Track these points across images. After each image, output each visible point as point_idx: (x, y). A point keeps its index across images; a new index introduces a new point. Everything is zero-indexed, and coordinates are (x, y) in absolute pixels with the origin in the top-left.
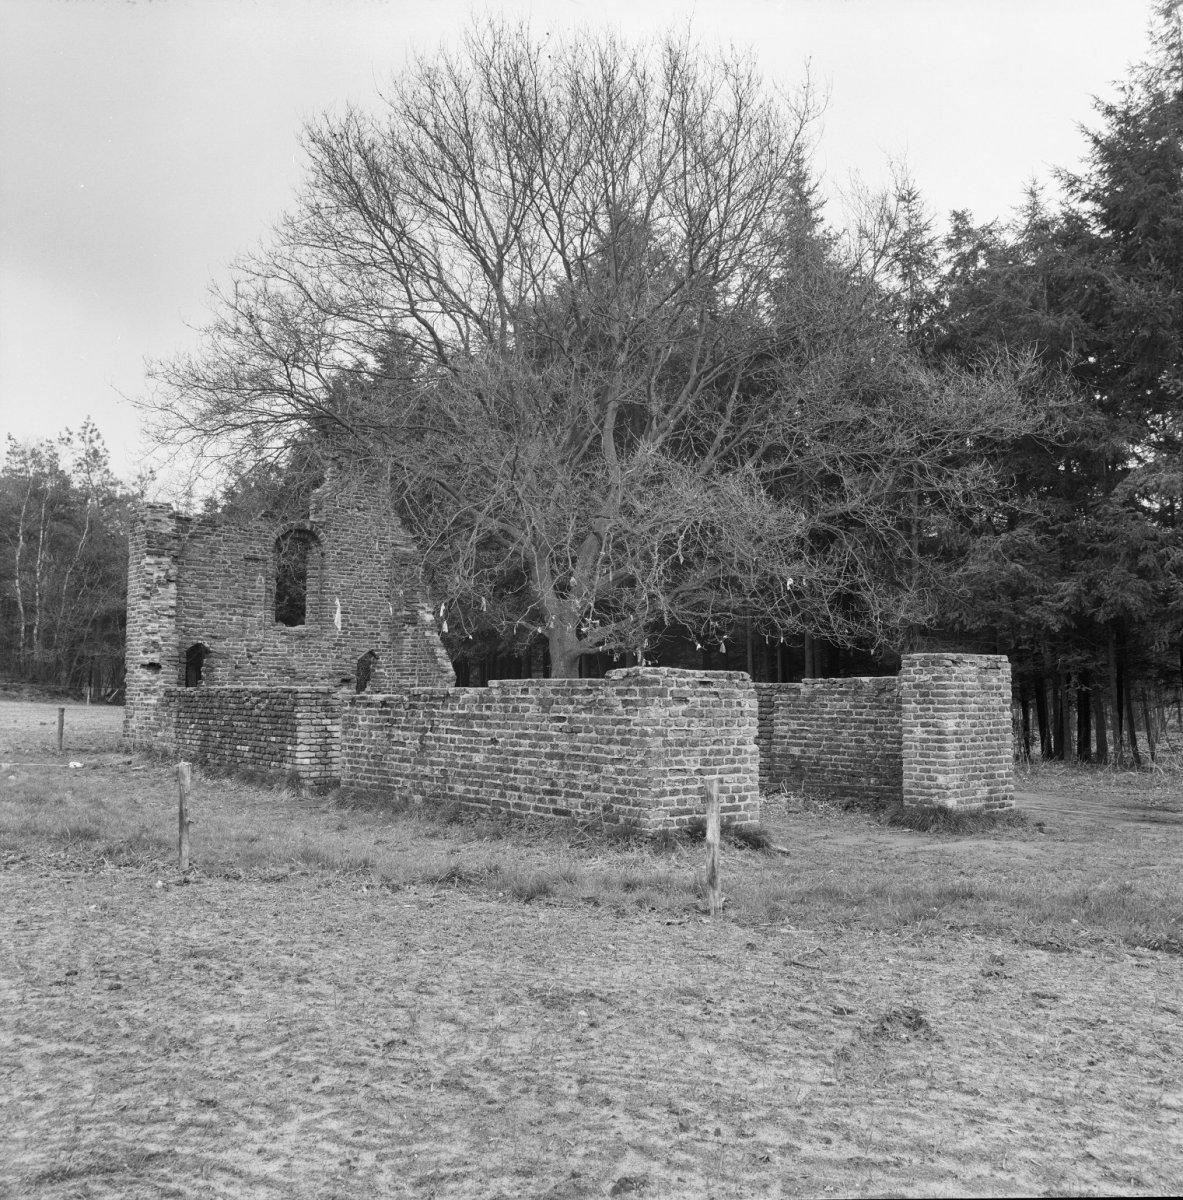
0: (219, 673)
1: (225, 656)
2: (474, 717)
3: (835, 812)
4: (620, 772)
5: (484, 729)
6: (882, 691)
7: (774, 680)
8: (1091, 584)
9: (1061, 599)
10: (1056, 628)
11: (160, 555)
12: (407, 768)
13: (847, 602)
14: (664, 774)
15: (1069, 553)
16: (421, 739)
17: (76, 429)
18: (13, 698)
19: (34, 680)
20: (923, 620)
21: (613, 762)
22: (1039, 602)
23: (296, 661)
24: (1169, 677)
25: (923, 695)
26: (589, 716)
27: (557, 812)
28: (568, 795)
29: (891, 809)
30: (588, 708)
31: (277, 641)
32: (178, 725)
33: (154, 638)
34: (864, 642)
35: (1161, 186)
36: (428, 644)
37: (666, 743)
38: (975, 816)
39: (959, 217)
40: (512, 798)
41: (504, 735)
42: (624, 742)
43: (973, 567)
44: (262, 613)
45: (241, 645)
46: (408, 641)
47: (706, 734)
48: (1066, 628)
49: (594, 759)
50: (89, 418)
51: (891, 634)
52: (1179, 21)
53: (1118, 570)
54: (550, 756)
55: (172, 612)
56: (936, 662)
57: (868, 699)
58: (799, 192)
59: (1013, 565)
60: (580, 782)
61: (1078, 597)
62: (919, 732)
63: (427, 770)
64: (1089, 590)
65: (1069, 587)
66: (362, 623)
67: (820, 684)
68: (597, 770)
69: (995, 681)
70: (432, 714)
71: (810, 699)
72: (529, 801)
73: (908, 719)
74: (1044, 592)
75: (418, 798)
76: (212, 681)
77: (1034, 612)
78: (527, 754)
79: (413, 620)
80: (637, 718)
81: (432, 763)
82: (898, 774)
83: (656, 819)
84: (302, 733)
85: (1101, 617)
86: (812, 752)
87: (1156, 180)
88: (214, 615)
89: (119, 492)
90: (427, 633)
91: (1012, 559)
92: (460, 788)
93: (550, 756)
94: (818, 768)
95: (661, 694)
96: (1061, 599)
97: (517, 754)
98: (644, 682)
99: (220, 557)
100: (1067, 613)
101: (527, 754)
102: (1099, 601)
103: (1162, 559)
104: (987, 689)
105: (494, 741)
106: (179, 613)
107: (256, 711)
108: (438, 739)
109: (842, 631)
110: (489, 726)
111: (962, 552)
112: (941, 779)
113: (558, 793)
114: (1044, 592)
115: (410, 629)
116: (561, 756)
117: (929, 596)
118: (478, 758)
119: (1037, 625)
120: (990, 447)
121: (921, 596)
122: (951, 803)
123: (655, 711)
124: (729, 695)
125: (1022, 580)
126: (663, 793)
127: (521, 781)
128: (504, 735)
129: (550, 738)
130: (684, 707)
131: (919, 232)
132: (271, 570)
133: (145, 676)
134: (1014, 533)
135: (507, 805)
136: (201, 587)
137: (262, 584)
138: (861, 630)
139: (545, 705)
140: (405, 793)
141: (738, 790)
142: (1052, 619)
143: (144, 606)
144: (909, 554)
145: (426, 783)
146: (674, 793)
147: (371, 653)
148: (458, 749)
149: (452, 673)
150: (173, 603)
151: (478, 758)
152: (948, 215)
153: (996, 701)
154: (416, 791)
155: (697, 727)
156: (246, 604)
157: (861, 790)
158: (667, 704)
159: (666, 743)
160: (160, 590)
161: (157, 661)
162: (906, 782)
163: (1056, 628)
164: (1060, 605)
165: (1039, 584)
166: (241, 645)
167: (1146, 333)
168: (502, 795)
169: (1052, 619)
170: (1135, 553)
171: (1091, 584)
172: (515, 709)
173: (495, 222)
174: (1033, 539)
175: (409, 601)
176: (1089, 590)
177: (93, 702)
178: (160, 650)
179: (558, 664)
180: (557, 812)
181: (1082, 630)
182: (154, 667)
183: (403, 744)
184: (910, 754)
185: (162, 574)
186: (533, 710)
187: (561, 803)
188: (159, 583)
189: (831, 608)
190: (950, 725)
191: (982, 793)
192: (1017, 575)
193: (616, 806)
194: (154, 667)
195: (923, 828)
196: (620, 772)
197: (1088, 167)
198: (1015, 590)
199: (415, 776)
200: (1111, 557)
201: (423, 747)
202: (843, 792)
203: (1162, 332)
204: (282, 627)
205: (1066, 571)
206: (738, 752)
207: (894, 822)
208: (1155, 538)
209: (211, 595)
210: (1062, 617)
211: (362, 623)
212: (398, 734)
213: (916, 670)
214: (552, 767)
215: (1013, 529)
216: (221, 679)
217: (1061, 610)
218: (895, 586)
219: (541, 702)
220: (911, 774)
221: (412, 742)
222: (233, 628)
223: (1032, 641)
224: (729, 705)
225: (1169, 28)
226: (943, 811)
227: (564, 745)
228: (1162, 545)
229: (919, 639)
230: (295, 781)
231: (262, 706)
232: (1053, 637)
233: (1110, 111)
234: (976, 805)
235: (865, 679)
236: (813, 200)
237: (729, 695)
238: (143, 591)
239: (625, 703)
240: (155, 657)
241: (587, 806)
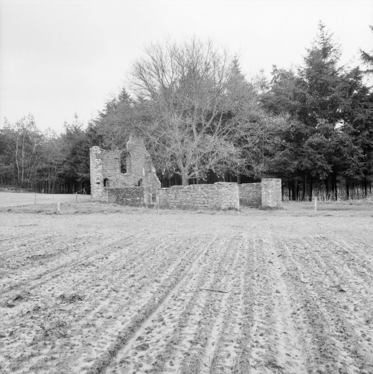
0: (110, 184)
1: (111, 181)
2: (187, 191)
3: (249, 209)
4: (217, 199)
5: (189, 193)
6: (258, 185)
7: (229, 181)
8: (300, 162)
9: (294, 165)
10: (293, 172)
11: (99, 158)
12: (172, 201)
13: (249, 167)
14: (224, 199)
15: (297, 155)
16: (175, 196)
17: (27, 116)
18: (19, 192)
19: (23, 187)
20: (265, 170)
21: (216, 198)
22: (290, 166)
23: (126, 181)
24: (372, 174)
25: (266, 186)
26: (211, 190)
27: (205, 207)
28: (207, 204)
29: (260, 207)
30: (211, 189)
31: (121, 177)
32: (109, 195)
33: (98, 177)
34: (253, 176)
35: (318, 73)
36: (154, 177)
37: (225, 194)
38: (274, 207)
39: (274, 66)
40: (196, 205)
41: (194, 194)
42: (218, 194)
43: (276, 158)
44: (119, 171)
45: (115, 178)
46: (149, 176)
47: (231, 193)
48: (295, 171)
49: (212, 197)
50: (65, 123)
51: (258, 173)
52: (323, 32)
53: (306, 159)
54: (203, 197)
55: (101, 171)
56: (268, 180)
57: (255, 187)
58: (236, 65)
59: (284, 158)
60: (209, 201)
61: (298, 166)
62: (265, 193)
63: (177, 201)
64: (300, 163)
65: (296, 163)
66: (139, 172)
67: (245, 184)
68: (213, 199)
69: (278, 184)
70: (178, 191)
71: (244, 187)
72: (199, 205)
73: (263, 191)
74: (291, 164)
75: (175, 206)
76: (109, 186)
77: (288, 168)
78: (199, 197)
79: (150, 172)
80: (220, 190)
81: (178, 200)
82: (261, 201)
83: (223, 207)
84: (145, 196)
85: (302, 169)
86: (244, 198)
87: (317, 71)
88: (109, 171)
89: (40, 134)
90: (154, 174)
91: (284, 156)
92: (184, 204)
93: (203, 197)
94: (245, 200)
95: (224, 186)
96: (294, 165)
97: (197, 197)
98: (221, 185)
99: (109, 158)
100: (295, 168)
101: (199, 197)
102: (302, 166)
103: (315, 157)
104: (277, 185)
105: (192, 195)
106: (103, 170)
107: (132, 192)
108: (179, 195)
109: (248, 173)
110: (191, 193)
111: (274, 154)
112: (269, 201)
113: (205, 203)
114: (291, 164)
115: (150, 174)
116: (206, 197)
117: (266, 165)
118: (188, 198)
119: (289, 171)
120: (279, 133)
121: (265, 164)
122: (270, 205)
123: (223, 189)
124: (234, 186)
125: (286, 161)
126: (224, 202)
127: (198, 202)
128: (194, 194)
129: (203, 194)
130: (227, 188)
131: (265, 79)
132: (120, 160)
133: (97, 185)
134: (285, 151)
135: (195, 206)
136: (106, 165)
137: (118, 165)
138: (252, 173)
139: (202, 189)
140: (172, 206)
141: (235, 202)
142: (292, 170)
143: (96, 170)
144: (262, 155)
145: (177, 203)
146: (226, 202)
147: (141, 179)
148: (184, 197)
149: (160, 183)
150: (101, 169)
151: (188, 198)
152: (272, 66)
153: (278, 187)
154: (174, 205)
155: (229, 192)
156: (115, 169)
157: (254, 204)
158: (225, 188)
159: (225, 194)
160: (99, 166)
161: (99, 182)
162: (262, 202)
163: (293, 172)
164: (294, 167)
165: (290, 162)
166: (115, 178)
167: (314, 107)
168: (194, 204)
169: (292, 170)
170: (309, 156)
171: (300, 162)
172: (196, 190)
173: (169, 81)
174: (289, 152)
175: (150, 168)
176: (300, 163)
177: (44, 193)
178: (100, 179)
179: (184, 181)
180: (205, 207)
181: (299, 172)
182: (98, 183)
183: (171, 197)
184: (263, 197)
185: (99, 163)
186: (200, 190)
187: (206, 205)
188: (99, 165)
189: (246, 168)
190: (270, 191)
191: (276, 203)
192: (285, 160)
193: (216, 205)
194: (98, 183)
195: (265, 210)
196: (217, 199)
197: (304, 66)
198: (285, 164)
199: (174, 202)
200: (305, 156)
201: (176, 197)
202: (250, 205)
203: (317, 107)
204: (122, 173)
205: (296, 159)
206: (235, 196)
207: (260, 209)
208: (314, 152)
209: (108, 167)
210: (294, 169)
211: (139, 172)
212: (170, 195)
213: (264, 182)
214: (204, 199)
215: (284, 150)
216: (111, 186)
217: (294, 168)
218: (259, 163)
219: (201, 188)
220: (263, 201)
221: (173, 196)
222: (113, 174)
223: (288, 175)
224: (234, 188)
225: (321, 33)
226: (269, 207)
227: (206, 195)
228: (315, 154)
229: (264, 174)
230: (144, 205)
231: (134, 191)
232: (292, 173)
233: (308, 50)
234: (275, 206)
235: (254, 183)
236: (239, 67)
237: (234, 186)
238: (96, 167)
239: (218, 188)
240: (98, 181)
241: (211, 205)
